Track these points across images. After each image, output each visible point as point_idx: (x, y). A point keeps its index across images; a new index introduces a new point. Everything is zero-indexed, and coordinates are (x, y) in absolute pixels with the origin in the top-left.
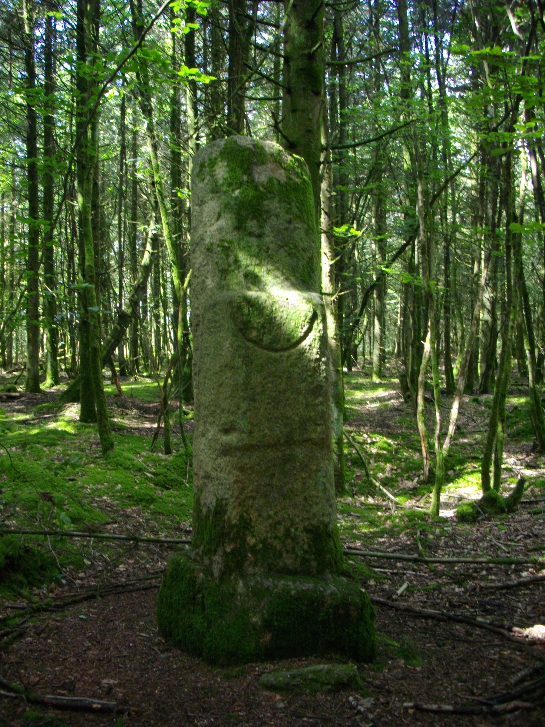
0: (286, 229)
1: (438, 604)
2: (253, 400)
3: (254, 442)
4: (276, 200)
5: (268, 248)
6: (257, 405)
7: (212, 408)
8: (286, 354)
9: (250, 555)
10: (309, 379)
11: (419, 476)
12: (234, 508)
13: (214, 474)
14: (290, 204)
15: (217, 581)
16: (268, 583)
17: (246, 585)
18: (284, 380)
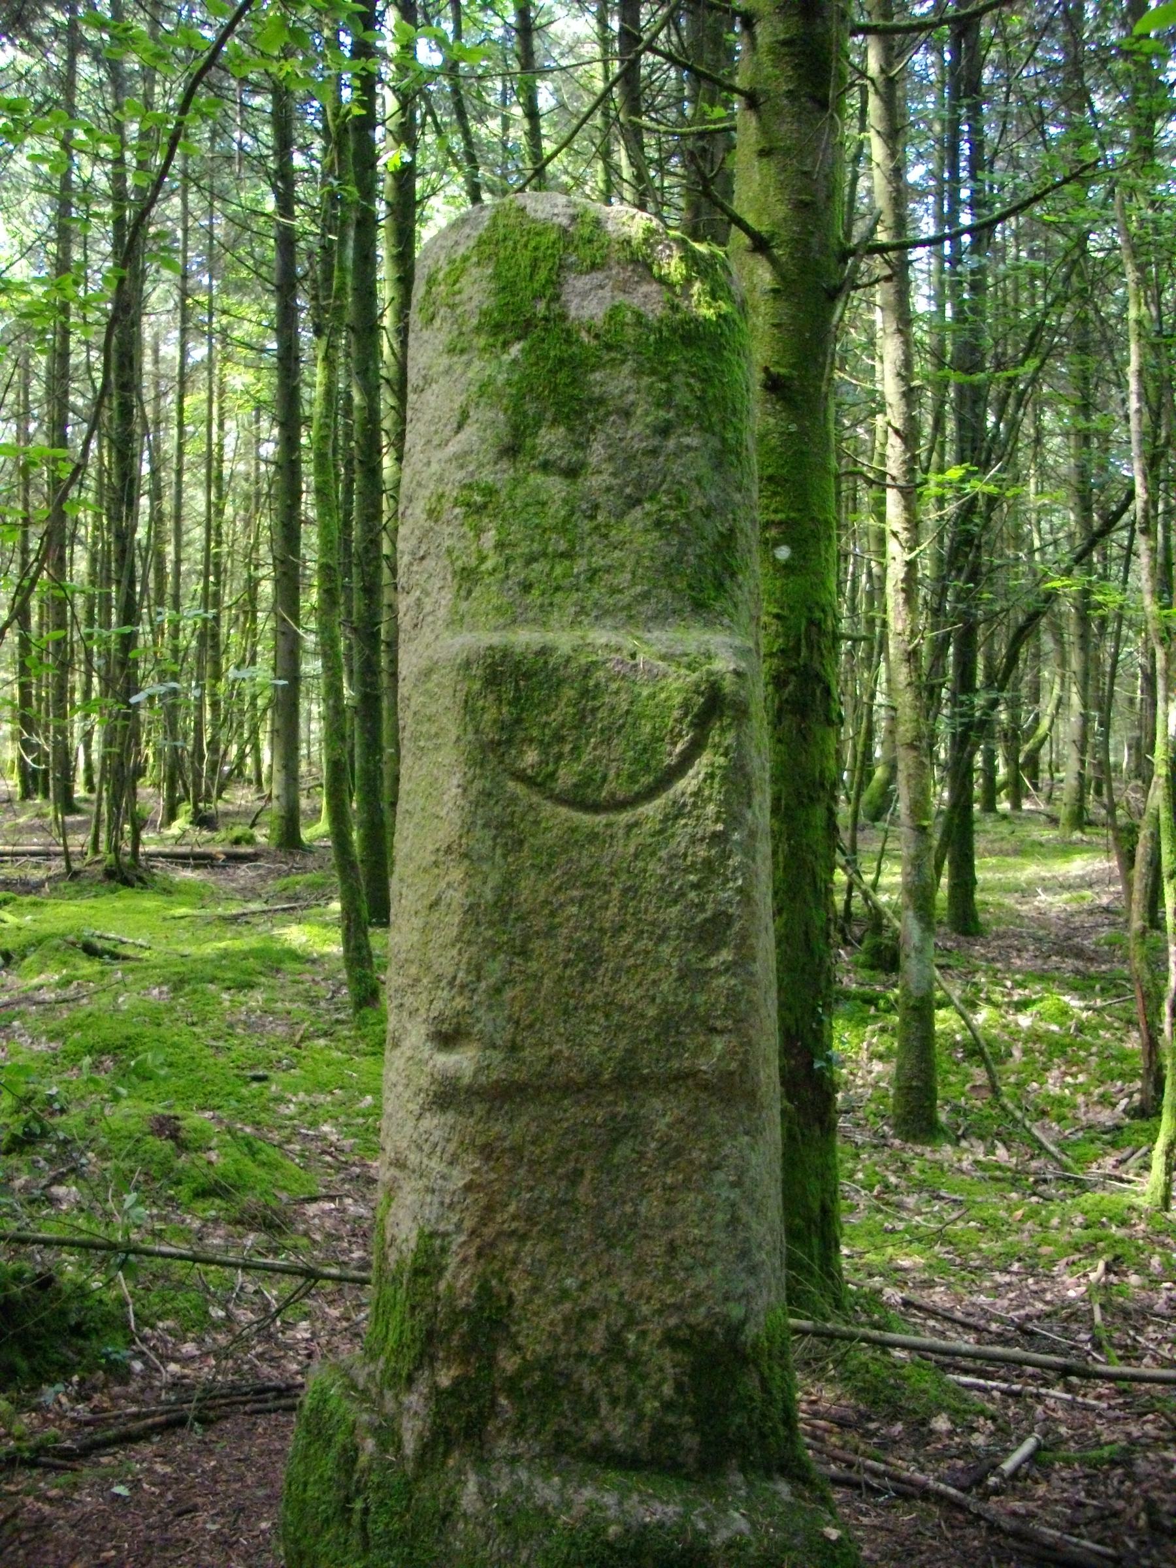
0: (654, 452)
1: (1116, 1514)
2: (524, 953)
3: (521, 1076)
4: (626, 369)
5: (596, 507)
6: (533, 966)
7: (413, 970)
8: (625, 817)
9: (503, 1401)
10: (692, 895)
11: (1130, 1096)
12: (464, 1261)
13: (413, 1158)
14: (667, 379)
15: (410, 1467)
16: (547, 1491)
17: (485, 1492)
18: (615, 893)
